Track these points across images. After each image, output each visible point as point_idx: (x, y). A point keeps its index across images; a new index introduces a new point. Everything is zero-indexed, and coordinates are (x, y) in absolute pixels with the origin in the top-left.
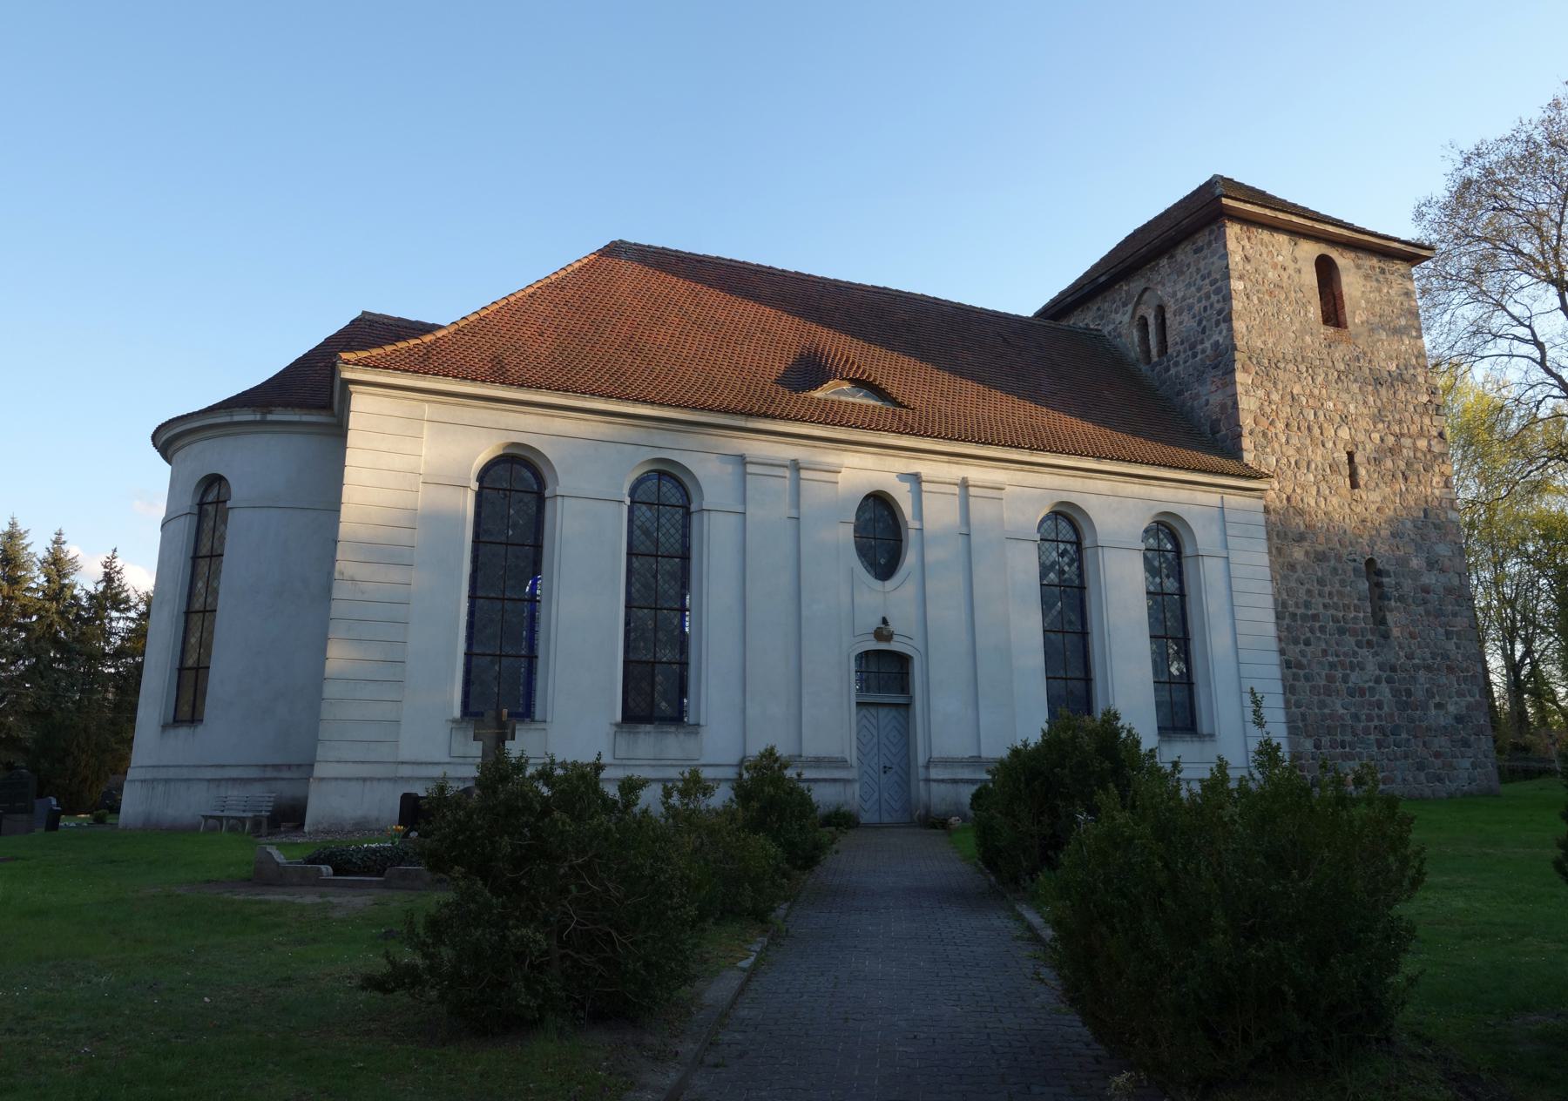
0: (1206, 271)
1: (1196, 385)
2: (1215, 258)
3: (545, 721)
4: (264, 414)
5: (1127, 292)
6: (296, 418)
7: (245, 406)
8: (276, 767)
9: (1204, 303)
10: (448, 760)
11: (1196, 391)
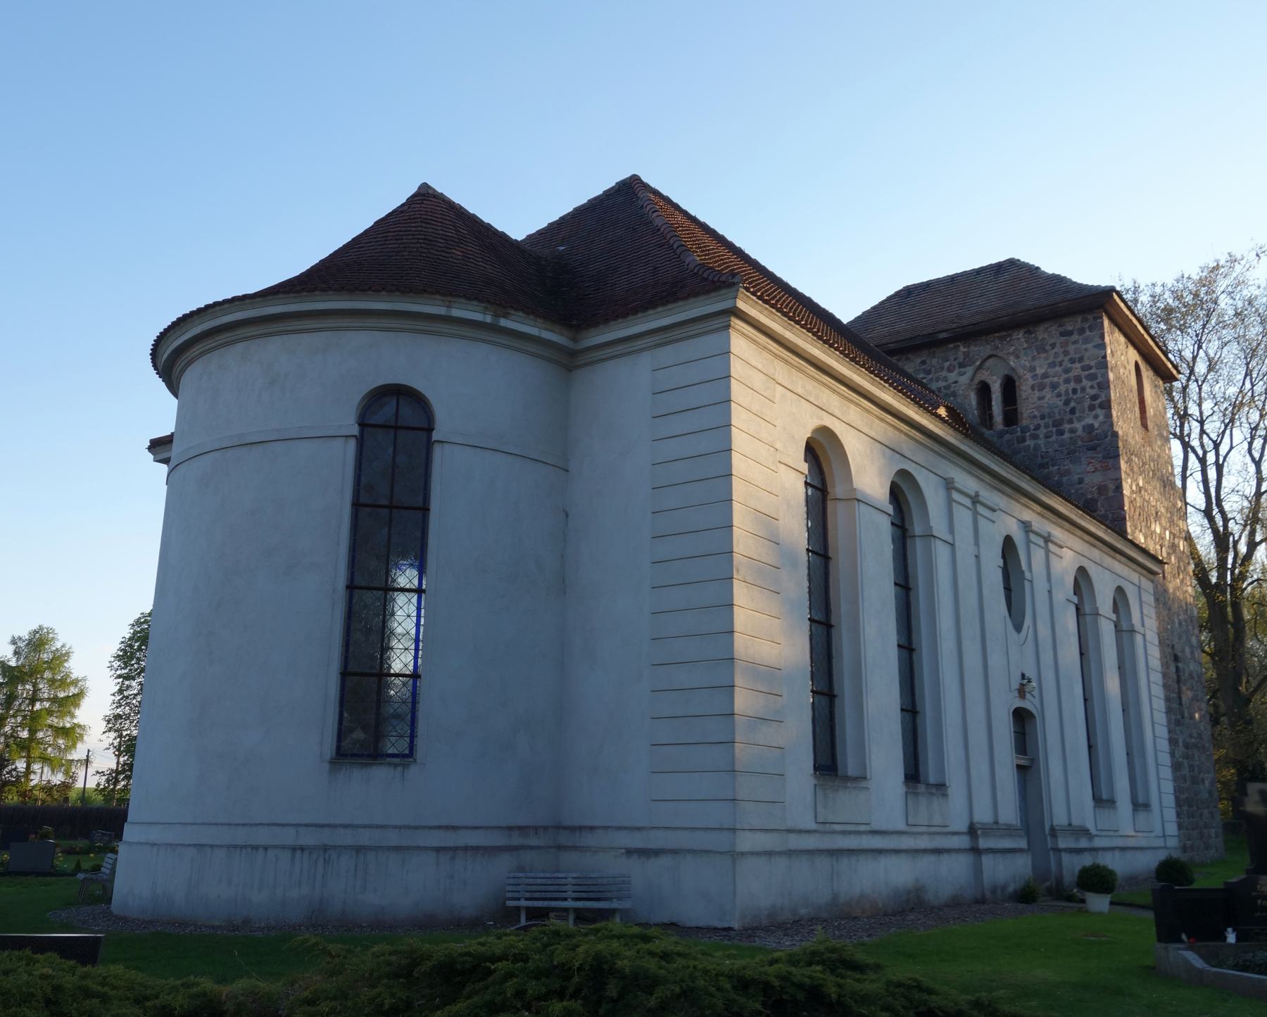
0: (1077, 356)
1: (1067, 462)
2: (1089, 346)
3: (865, 778)
4: (496, 316)
5: (966, 355)
6: (534, 331)
7: (438, 292)
8: (522, 829)
9: (1072, 385)
10: (813, 826)
11: (1066, 467)
